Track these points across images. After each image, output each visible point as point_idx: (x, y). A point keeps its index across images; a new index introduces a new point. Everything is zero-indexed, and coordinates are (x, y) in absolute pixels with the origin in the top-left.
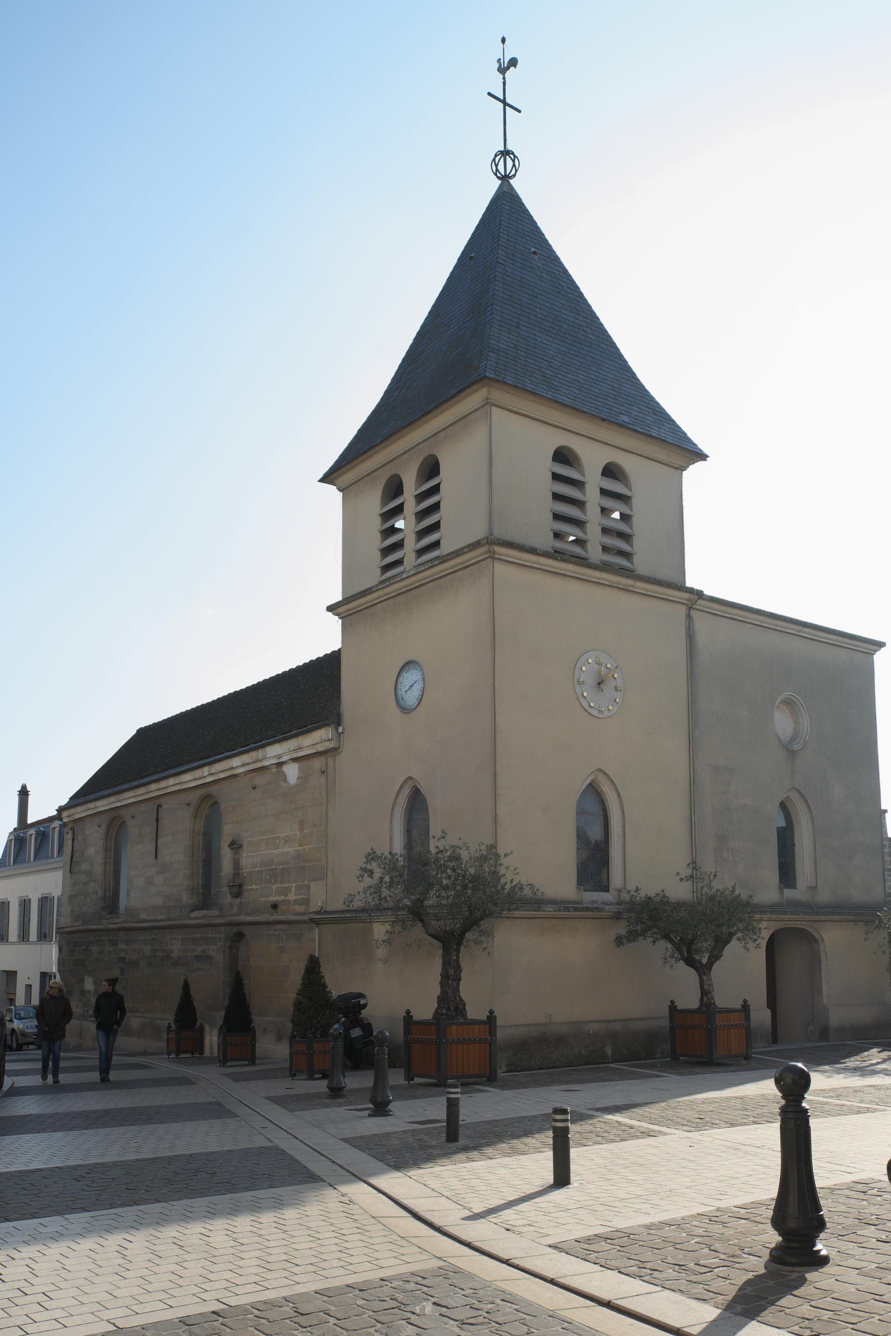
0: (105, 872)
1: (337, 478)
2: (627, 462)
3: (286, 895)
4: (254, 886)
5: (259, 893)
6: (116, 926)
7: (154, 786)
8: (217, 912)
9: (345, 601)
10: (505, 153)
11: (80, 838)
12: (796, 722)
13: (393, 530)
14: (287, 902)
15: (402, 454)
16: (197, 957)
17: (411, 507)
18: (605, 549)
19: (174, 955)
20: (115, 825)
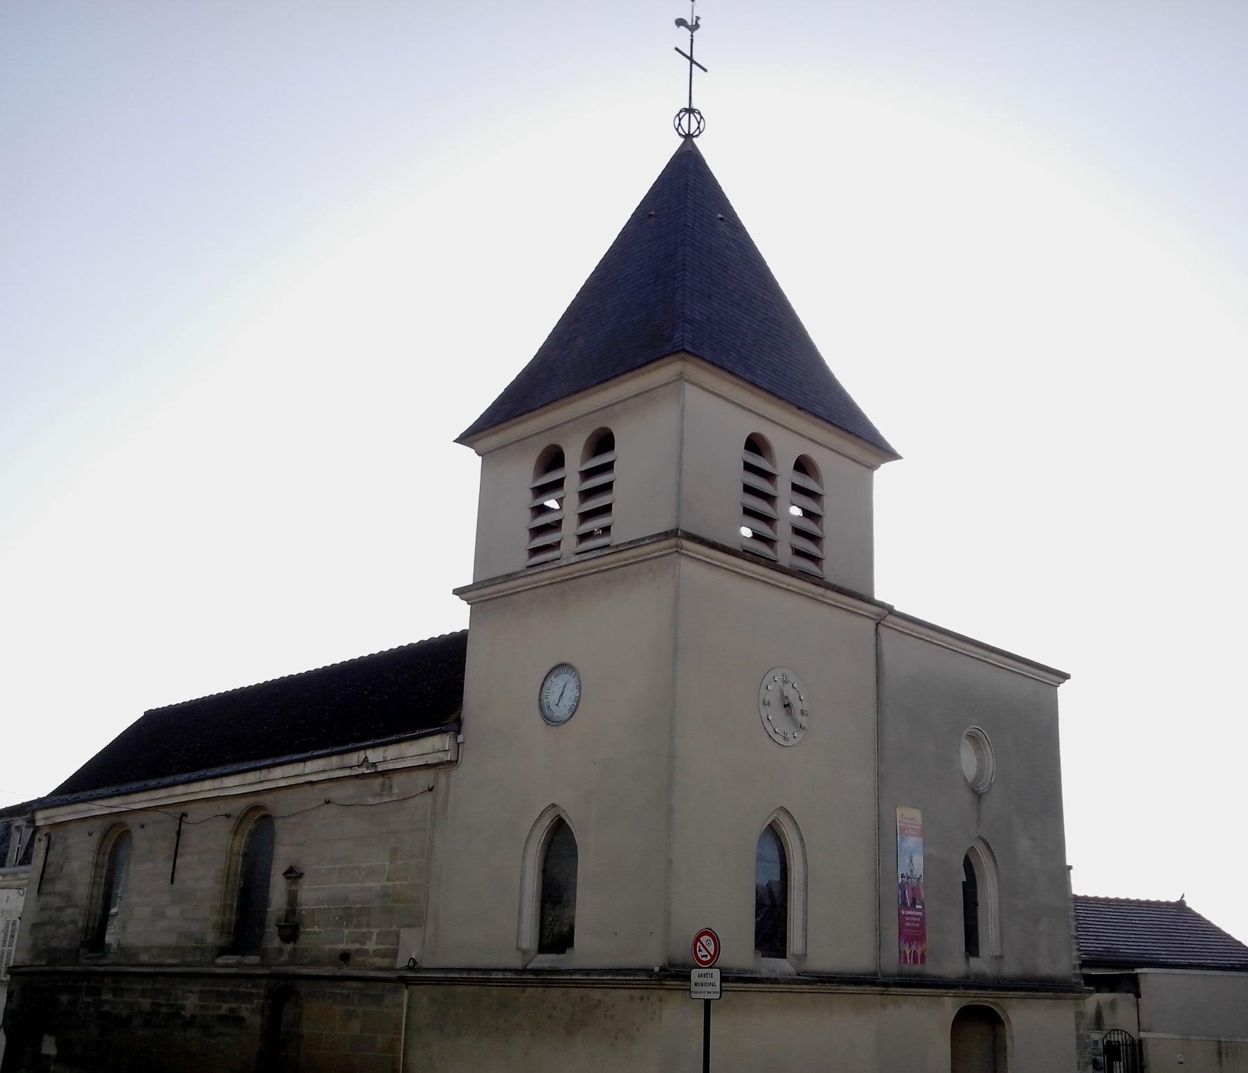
0: (91, 897)
1: (477, 440)
2: (819, 456)
3: (364, 944)
4: (316, 929)
5: (322, 938)
6: (102, 969)
7: (180, 789)
8: (255, 959)
9: (478, 585)
10: (690, 111)
11: (58, 847)
12: (980, 760)
13: (542, 510)
14: (364, 952)
15: (568, 423)
16: (222, 1019)
17: (574, 483)
18: (798, 552)
19: (186, 1013)
20: (116, 836)
